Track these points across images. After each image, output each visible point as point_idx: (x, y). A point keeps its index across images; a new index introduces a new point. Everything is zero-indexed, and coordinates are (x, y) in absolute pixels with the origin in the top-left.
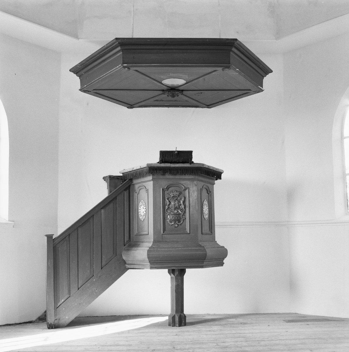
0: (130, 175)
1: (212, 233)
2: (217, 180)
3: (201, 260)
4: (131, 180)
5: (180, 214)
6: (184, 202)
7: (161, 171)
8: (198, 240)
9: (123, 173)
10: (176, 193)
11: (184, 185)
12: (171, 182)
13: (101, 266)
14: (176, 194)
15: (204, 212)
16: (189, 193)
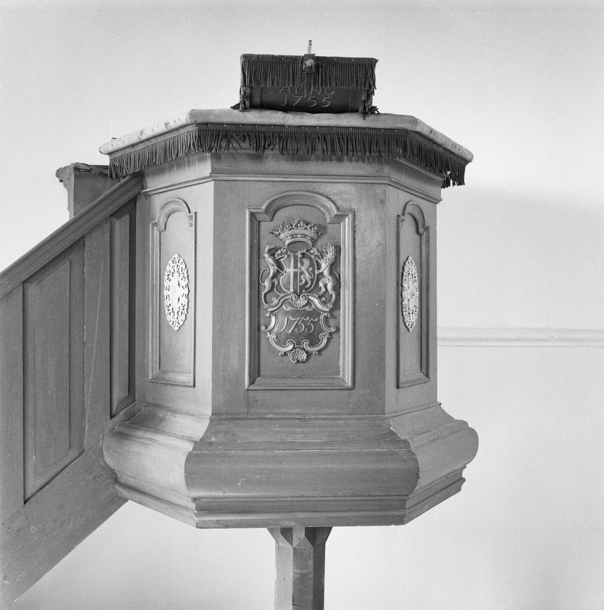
0: (132, 157)
1: (427, 375)
2: (446, 184)
3: (394, 497)
4: (139, 177)
5: (316, 313)
6: (334, 266)
7: (247, 140)
8: (383, 412)
9: (110, 154)
10: (306, 232)
11: (335, 198)
12: (285, 189)
13: (111, 412)
14: (305, 236)
15: (405, 302)
16: (354, 232)
